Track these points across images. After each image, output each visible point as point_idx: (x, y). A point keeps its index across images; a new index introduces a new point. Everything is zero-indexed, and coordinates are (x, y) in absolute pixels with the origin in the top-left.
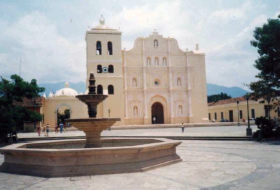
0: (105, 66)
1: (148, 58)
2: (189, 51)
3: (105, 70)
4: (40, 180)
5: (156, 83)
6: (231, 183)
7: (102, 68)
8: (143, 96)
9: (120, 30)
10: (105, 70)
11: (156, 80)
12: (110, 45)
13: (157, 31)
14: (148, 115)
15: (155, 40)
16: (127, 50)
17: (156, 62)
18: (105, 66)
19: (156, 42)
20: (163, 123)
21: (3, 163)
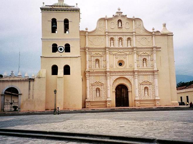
0: (61, 45)
1: (112, 39)
2: (155, 30)
3: (61, 49)
4: (137, 135)
5: (120, 64)
6: (29, 126)
7: (58, 46)
8: (106, 79)
9: (79, 7)
10: (61, 49)
11: (119, 61)
12: (66, 22)
13: (121, 11)
14: (111, 97)
15: (119, 20)
16: (89, 30)
17: (120, 43)
18: (61, 45)
19: (120, 23)
20: (128, 106)
21: (157, 143)
